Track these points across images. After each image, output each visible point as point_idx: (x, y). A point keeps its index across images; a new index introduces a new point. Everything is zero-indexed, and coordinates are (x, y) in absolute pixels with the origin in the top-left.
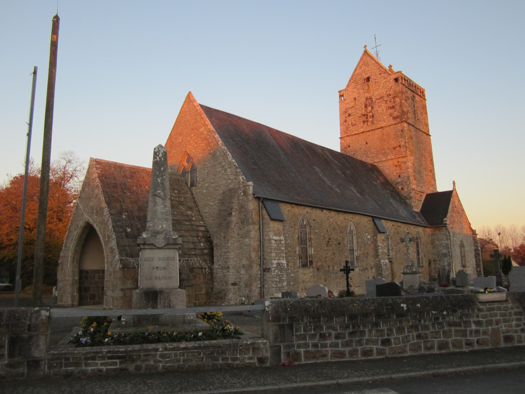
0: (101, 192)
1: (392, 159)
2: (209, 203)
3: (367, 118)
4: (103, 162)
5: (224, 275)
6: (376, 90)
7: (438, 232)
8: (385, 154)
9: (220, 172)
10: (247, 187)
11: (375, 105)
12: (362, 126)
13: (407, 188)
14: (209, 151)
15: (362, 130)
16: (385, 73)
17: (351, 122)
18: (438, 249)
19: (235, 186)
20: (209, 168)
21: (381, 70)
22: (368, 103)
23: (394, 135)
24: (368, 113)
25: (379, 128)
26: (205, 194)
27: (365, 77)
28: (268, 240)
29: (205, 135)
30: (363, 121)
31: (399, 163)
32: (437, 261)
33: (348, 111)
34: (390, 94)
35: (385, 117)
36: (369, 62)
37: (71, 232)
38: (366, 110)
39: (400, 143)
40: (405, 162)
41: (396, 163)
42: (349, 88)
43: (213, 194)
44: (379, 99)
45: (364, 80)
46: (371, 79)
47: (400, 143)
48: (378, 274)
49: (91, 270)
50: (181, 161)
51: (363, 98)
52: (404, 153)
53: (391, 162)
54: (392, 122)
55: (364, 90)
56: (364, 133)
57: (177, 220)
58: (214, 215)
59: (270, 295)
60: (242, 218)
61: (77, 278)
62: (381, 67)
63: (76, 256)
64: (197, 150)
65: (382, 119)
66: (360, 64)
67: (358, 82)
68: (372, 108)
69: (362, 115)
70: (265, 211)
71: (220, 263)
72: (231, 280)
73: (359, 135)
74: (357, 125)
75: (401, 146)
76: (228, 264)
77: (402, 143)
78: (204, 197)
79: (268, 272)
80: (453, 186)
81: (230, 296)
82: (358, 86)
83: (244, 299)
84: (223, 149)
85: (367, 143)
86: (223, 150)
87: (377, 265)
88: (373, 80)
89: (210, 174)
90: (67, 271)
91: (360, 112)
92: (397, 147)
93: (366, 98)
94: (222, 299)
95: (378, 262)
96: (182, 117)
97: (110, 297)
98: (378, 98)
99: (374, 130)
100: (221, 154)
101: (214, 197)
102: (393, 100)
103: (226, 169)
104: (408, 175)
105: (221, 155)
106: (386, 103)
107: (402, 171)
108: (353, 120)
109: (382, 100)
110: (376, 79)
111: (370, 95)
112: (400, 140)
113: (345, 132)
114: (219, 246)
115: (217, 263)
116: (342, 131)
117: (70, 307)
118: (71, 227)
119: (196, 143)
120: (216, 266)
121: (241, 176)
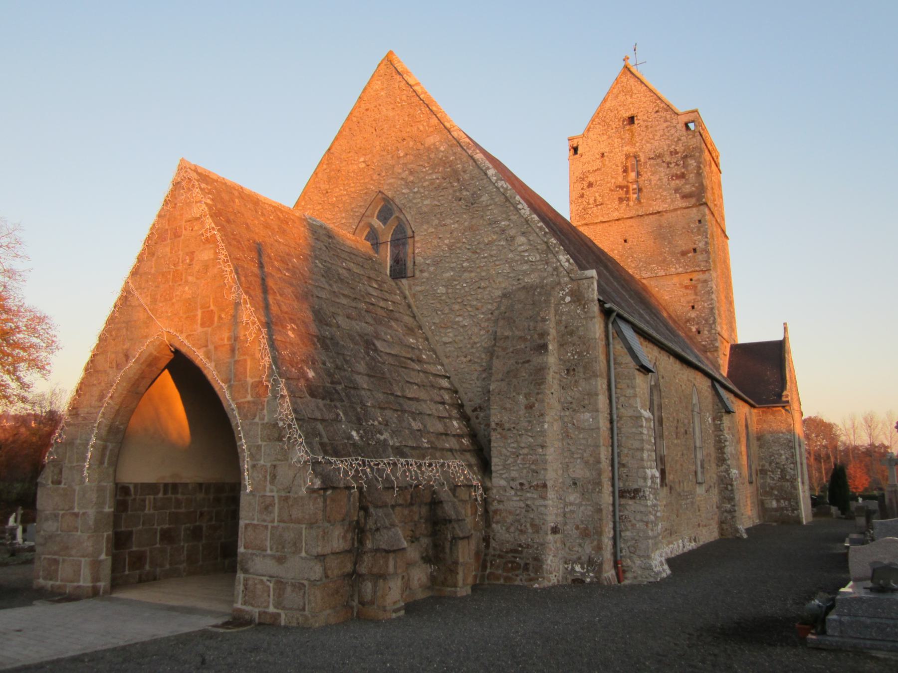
0: (226, 256)
1: (678, 274)
2: (457, 319)
3: (627, 192)
4: (215, 177)
5: (527, 505)
6: (648, 142)
7: (772, 417)
8: (663, 263)
9: (490, 243)
10: (584, 281)
11: (645, 170)
12: (617, 207)
13: (709, 331)
14: (455, 191)
15: (616, 215)
16: (667, 111)
17: (593, 198)
18: (771, 450)
19: (545, 278)
20: (455, 234)
21: (658, 104)
22: (629, 164)
23: (684, 228)
24: (629, 184)
25: (652, 214)
26: (444, 298)
27: (624, 116)
28: (630, 417)
29: (442, 154)
30: (619, 198)
31: (693, 282)
32: (769, 473)
33: (587, 177)
34: (676, 150)
35: (665, 193)
36: (633, 88)
37: (97, 372)
38: (625, 178)
39: (695, 244)
40: (705, 281)
41: (687, 282)
42: (591, 134)
43: (469, 298)
44: (652, 158)
45: (623, 121)
46: (637, 119)
47: (695, 244)
48: (725, 498)
49: (136, 485)
50: (363, 215)
51: (620, 154)
52: (703, 264)
53: (676, 280)
54: (680, 203)
55: (622, 139)
56: (620, 222)
57: (396, 356)
58: (474, 350)
59: (639, 556)
60: (569, 360)
61: (108, 509)
62: (660, 98)
63: (110, 446)
64: (416, 190)
65: (659, 196)
66: (615, 91)
67: (611, 123)
68: (638, 174)
69: (617, 187)
70: (622, 344)
71: (514, 474)
72: (551, 520)
73: (610, 223)
74: (607, 204)
75: (698, 251)
76: (541, 477)
77: (700, 245)
78: (439, 306)
79: (634, 498)
80: (785, 333)
81: (549, 562)
82: (611, 132)
83: (578, 568)
84: (502, 187)
85: (625, 241)
86: (502, 190)
87: (722, 480)
88: (642, 123)
89: (460, 248)
90: (77, 488)
91: (613, 181)
92: (688, 252)
93: (626, 155)
94: (526, 567)
95: (724, 474)
96: (367, 110)
97: (265, 579)
98: (653, 156)
99: (641, 216)
100: (497, 200)
101: (471, 306)
102: (682, 162)
103: (513, 238)
104: (710, 306)
105: (495, 204)
106: (668, 167)
107: (699, 298)
108: (597, 195)
109: (659, 161)
110: (647, 121)
111: (634, 150)
112: (695, 238)
113: (580, 216)
114: (509, 430)
115: (501, 474)
116: (573, 214)
117: (88, 597)
118: (98, 357)
119: (411, 173)
120: (498, 481)
121: (563, 255)
